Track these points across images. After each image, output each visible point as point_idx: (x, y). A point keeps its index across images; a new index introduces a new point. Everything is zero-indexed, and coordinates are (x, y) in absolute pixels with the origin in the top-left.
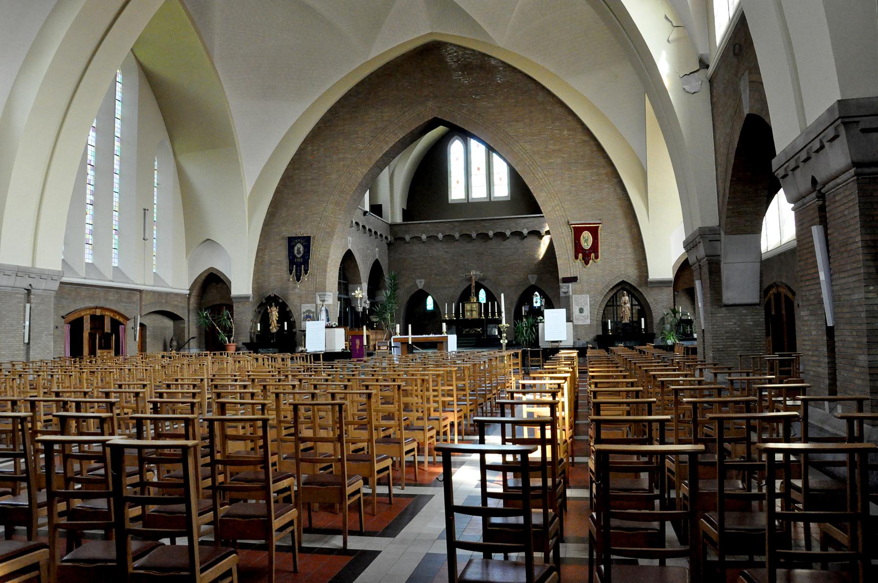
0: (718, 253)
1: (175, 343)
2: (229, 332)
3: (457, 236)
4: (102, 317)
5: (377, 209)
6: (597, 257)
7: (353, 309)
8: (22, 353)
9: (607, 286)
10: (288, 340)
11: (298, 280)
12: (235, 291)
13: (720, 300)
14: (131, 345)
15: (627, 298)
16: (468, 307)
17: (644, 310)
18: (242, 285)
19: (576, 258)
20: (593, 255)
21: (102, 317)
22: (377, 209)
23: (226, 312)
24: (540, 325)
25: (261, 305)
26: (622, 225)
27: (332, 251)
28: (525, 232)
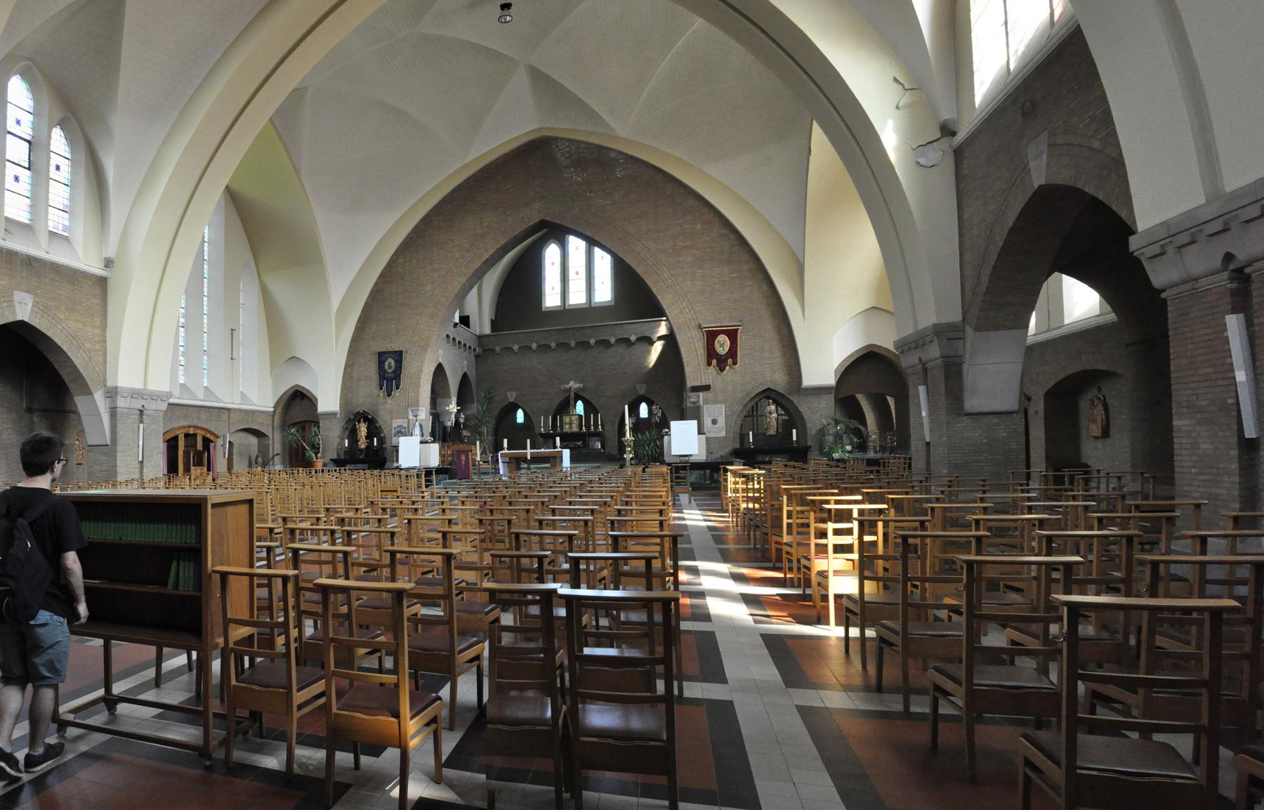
0: (960, 353)
1: (260, 460)
2: (316, 448)
3: (553, 345)
4: (195, 435)
5: (465, 320)
6: (735, 363)
7: (441, 423)
8: (137, 470)
9: (747, 394)
10: (376, 456)
11: (389, 395)
12: (322, 407)
13: (962, 408)
14: (220, 464)
15: (773, 407)
16: (567, 419)
17: (793, 418)
18: (329, 400)
19: (709, 364)
20: (730, 361)
21: (195, 435)
22: (465, 320)
23: (314, 429)
24: (666, 438)
25: (349, 421)
26: (769, 326)
27: (426, 364)
28: (633, 338)
